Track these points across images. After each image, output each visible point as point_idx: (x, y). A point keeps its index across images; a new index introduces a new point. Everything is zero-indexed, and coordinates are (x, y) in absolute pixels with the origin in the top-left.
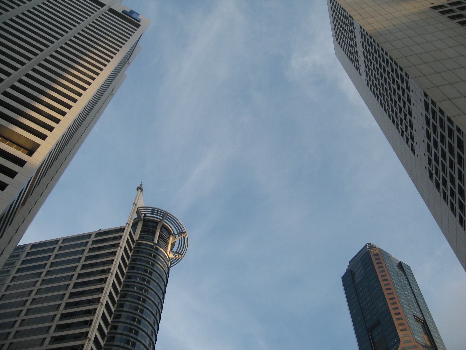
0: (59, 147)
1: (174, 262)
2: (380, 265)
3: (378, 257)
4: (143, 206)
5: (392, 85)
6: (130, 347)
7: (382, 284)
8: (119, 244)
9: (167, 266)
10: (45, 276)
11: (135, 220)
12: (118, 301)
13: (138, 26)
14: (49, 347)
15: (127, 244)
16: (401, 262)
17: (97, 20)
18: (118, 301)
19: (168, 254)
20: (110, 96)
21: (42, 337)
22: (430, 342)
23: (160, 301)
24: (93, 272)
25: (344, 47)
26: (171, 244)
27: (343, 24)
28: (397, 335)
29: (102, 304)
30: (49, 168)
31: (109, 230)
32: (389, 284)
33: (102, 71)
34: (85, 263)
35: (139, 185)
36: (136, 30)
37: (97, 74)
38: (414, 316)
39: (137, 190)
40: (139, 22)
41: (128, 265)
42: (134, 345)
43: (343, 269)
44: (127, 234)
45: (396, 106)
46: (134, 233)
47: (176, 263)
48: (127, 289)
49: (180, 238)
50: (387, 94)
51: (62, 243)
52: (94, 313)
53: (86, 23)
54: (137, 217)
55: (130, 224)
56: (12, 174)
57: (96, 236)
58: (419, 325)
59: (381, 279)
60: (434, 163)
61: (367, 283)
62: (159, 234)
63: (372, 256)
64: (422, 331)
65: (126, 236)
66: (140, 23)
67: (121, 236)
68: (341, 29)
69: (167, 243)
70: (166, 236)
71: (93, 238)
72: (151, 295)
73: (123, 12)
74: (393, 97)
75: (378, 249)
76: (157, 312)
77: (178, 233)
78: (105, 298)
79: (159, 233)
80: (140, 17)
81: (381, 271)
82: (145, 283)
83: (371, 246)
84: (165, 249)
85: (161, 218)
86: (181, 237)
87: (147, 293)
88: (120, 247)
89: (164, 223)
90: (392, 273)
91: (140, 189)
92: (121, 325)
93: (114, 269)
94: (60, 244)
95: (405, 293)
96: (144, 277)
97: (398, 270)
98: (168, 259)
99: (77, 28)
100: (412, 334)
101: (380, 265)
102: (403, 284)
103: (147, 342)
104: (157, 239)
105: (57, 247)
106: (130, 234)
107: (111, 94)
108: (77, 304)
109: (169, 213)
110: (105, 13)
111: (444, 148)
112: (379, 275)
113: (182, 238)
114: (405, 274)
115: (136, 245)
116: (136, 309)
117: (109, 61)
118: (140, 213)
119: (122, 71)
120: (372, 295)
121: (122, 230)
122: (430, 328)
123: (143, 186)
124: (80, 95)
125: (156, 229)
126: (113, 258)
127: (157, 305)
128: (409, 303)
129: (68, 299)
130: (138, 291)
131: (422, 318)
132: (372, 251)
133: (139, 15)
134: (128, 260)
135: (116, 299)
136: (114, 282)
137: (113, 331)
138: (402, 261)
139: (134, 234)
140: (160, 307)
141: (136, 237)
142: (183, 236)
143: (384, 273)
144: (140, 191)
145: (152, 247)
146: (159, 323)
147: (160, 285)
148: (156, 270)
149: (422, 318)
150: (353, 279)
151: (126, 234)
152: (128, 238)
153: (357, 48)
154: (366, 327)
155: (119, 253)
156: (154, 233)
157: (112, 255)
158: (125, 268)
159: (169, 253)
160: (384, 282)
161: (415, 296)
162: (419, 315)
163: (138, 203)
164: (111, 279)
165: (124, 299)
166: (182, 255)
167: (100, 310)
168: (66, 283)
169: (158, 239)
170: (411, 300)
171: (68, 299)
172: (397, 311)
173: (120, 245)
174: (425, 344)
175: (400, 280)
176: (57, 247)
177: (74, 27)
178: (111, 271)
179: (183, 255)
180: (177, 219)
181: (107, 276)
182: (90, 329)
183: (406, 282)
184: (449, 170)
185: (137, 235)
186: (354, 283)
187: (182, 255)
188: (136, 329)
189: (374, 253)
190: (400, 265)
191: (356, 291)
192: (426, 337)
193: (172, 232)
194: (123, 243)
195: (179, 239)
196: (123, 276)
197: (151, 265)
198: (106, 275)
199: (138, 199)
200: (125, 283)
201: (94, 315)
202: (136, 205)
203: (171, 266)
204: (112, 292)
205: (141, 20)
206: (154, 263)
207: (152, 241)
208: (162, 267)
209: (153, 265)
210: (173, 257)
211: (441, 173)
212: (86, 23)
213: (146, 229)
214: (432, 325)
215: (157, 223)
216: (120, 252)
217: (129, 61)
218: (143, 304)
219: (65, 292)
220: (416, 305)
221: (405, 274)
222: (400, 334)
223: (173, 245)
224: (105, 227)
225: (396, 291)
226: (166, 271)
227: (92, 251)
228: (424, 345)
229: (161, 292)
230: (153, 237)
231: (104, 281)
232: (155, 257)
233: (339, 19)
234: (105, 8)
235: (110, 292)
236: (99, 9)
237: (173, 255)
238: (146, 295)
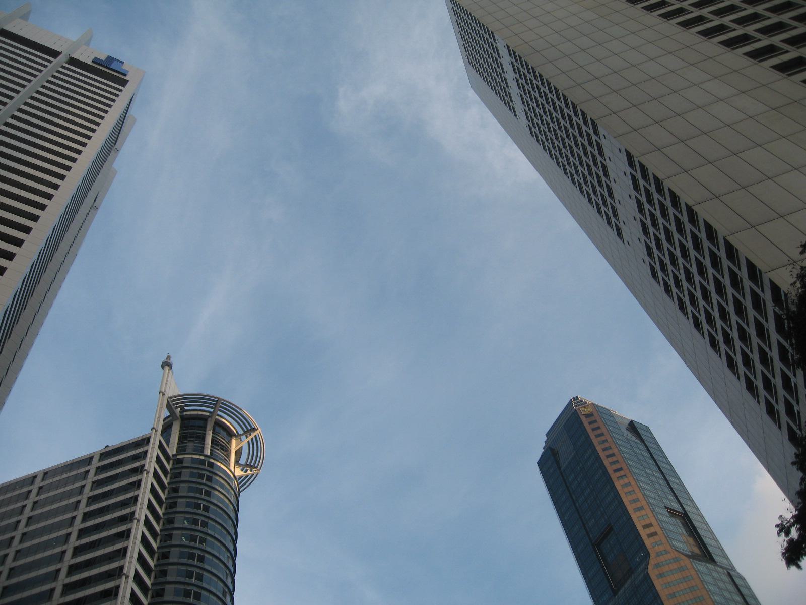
0: (24, 296)
1: (245, 482)
2: (599, 432)
3: (592, 419)
4: (177, 393)
5: (574, 119)
6: (192, 601)
7: (606, 462)
8: (143, 466)
9: (232, 492)
10: (42, 481)
11: (166, 421)
12: (166, 499)
13: (124, 83)
14: (62, 600)
15: (158, 464)
16: (632, 421)
17: (49, 81)
18: (155, 566)
19: (233, 471)
20: (92, 209)
21: (75, 501)
22: (700, 548)
23: (229, 555)
24: (95, 558)
25: (480, 61)
26: (236, 452)
27: (477, 25)
28: (642, 545)
29: (127, 577)
30: (15, 324)
31: (123, 444)
32: (617, 461)
33: (28, 234)
34: (78, 543)
35: (164, 359)
36: (121, 91)
37: (35, 218)
38: (666, 508)
39: (163, 367)
40: (125, 75)
41: (167, 486)
42: (198, 597)
43: (538, 451)
44: (155, 447)
45: (586, 154)
46: (168, 444)
47: (246, 485)
48: (175, 494)
49: (249, 439)
50: (568, 136)
51: (43, 480)
52: (116, 595)
53: (35, 83)
54: (169, 414)
55: (159, 430)
56: (10, 256)
57: (100, 460)
58: (678, 522)
59: (602, 455)
60: (651, 230)
61: (581, 465)
62: (212, 439)
63: (583, 418)
64: (684, 532)
65: (153, 451)
66: (126, 78)
67: (146, 452)
68: (478, 38)
69: (228, 451)
70: (224, 440)
71: (96, 463)
72: (212, 547)
73: (93, 62)
74: (589, 148)
75: (590, 404)
76: (227, 574)
77: (245, 432)
78: (131, 565)
79: (211, 436)
80: (125, 67)
81: (602, 442)
82: (199, 528)
83: (578, 402)
84: (226, 464)
85: (212, 410)
86: (251, 437)
87: (204, 544)
88: (145, 473)
89: (217, 417)
90: (620, 443)
91: (168, 366)
92: (179, 517)
93: (141, 511)
94: (38, 483)
95: (646, 473)
96: (197, 501)
97: (630, 435)
98: (234, 479)
99: (14, 100)
100: (668, 538)
101: (599, 432)
102: (641, 458)
103: (218, 588)
104: (209, 447)
105: (35, 488)
106: (161, 446)
107: (94, 206)
108: (89, 564)
109: (223, 400)
110: (63, 67)
111: (679, 216)
112: (599, 448)
113: (252, 439)
114: (643, 441)
115: (173, 464)
116: (198, 506)
117: (84, 145)
118: (173, 407)
119: (106, 165)
120: (603, 508)
121: (146, 441)
122: (696, 524)
123: (171, 359)
124: (35, 218)
125: (205, 431)
126: (136, 493)
127: (226, 562)
128: (655, 488)
129: (67, 577)
130: (187, 543)
131: (680, 510)
132: (582, 409)
133: (123, 63)
134: (163, 491)
135: (152, 563)
136: (143, 534)
137: (169, 526)
138: (634, 419)
139: (168, 445)
140: (229, 583)
141: (172, 450)
142: (253, 435)
143: (606, 445)
144: (167, 368)
145: (202, 462)
146: (235, 575)
147: (224, 542)
148: (215, 502)
149: (680, 510)
150: (558, 463)
151: (153, 448)
152: (160, 440)
153: (501, 57)
154: (590, 539)
155: (152, 453)
156: (203, 438)
157: (124, 537)
158: (161, 506)
159: (234, 468)
160: (609, 459)
161: (663, 474)
162: (676, 506)
163: (167, 390)
164: (138, 530)
165: (178, 480)
166: (256, 468)
167: (126, 587)
168: (58, 550)
169: (211, 446)
170: (658, 483)
171: (67, 577)
172: (610, 452)
173: (146, 468)
174: (690, 552)
175: (634, 452)
176: (35, 488)
177: (39, 73)
178: (136, 515)
179: (259, 468)
180: (239, 407)
181: (129, 526)
182: (121, 581)
183: (646, 454)
184: (693, 253)
185: (174, 446)
186: (559, 468)
187: (256, 468)
188: (196, 589)
189: (585, 413)
190: (633, 427)
191: (581, 517)
192: (691, 540)
193: (233, 431)
194: (151, 464)
195: (248, 442)
196: (160, 505)
197: (206, 480)
198: (127, 524)
199: (166, 383)
200: (158, 569)
201: (117, 599)
202: (164, 394)
203: (241, 490)
204: (139, 571)
205: (128, 71)
206: (209, 489)
207: (201, 451)
208: (224, 495)
209: (208, 494)
210: (243, 473)
211: (681, 261)
212: (35, 83)
213: (187, 433)
214: (699, 518)
215: (205, 419)
216: (148, 480)
217: (116, 146)
218: (199, 583)
219: (69, 530)
220: (667, 490)
221: (643, 441)
222: (648, 542)
223: (239, 453)
224: (115, 442)
225: (639, 486)
226: (233, 500)
227: (93, 501)
228: (690, 554)
229: (230, 538)
230: (204, 432)
231: (126, 535)
232: (209, 479)
233: (465, 15)
234: (62, 59)
235: (143, 535)
236: (50, 62)
237: (242, 470)
238: (204, 549)
